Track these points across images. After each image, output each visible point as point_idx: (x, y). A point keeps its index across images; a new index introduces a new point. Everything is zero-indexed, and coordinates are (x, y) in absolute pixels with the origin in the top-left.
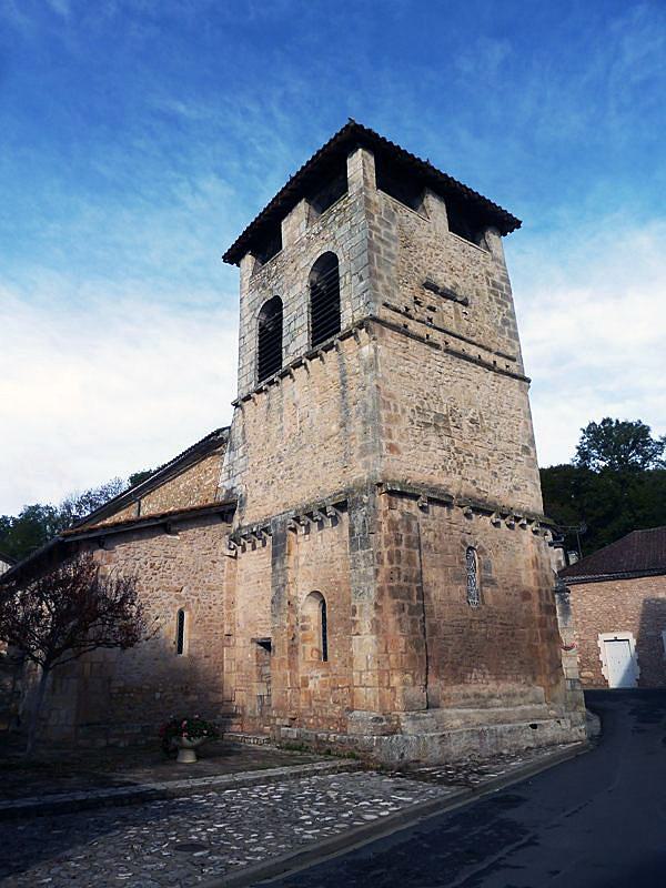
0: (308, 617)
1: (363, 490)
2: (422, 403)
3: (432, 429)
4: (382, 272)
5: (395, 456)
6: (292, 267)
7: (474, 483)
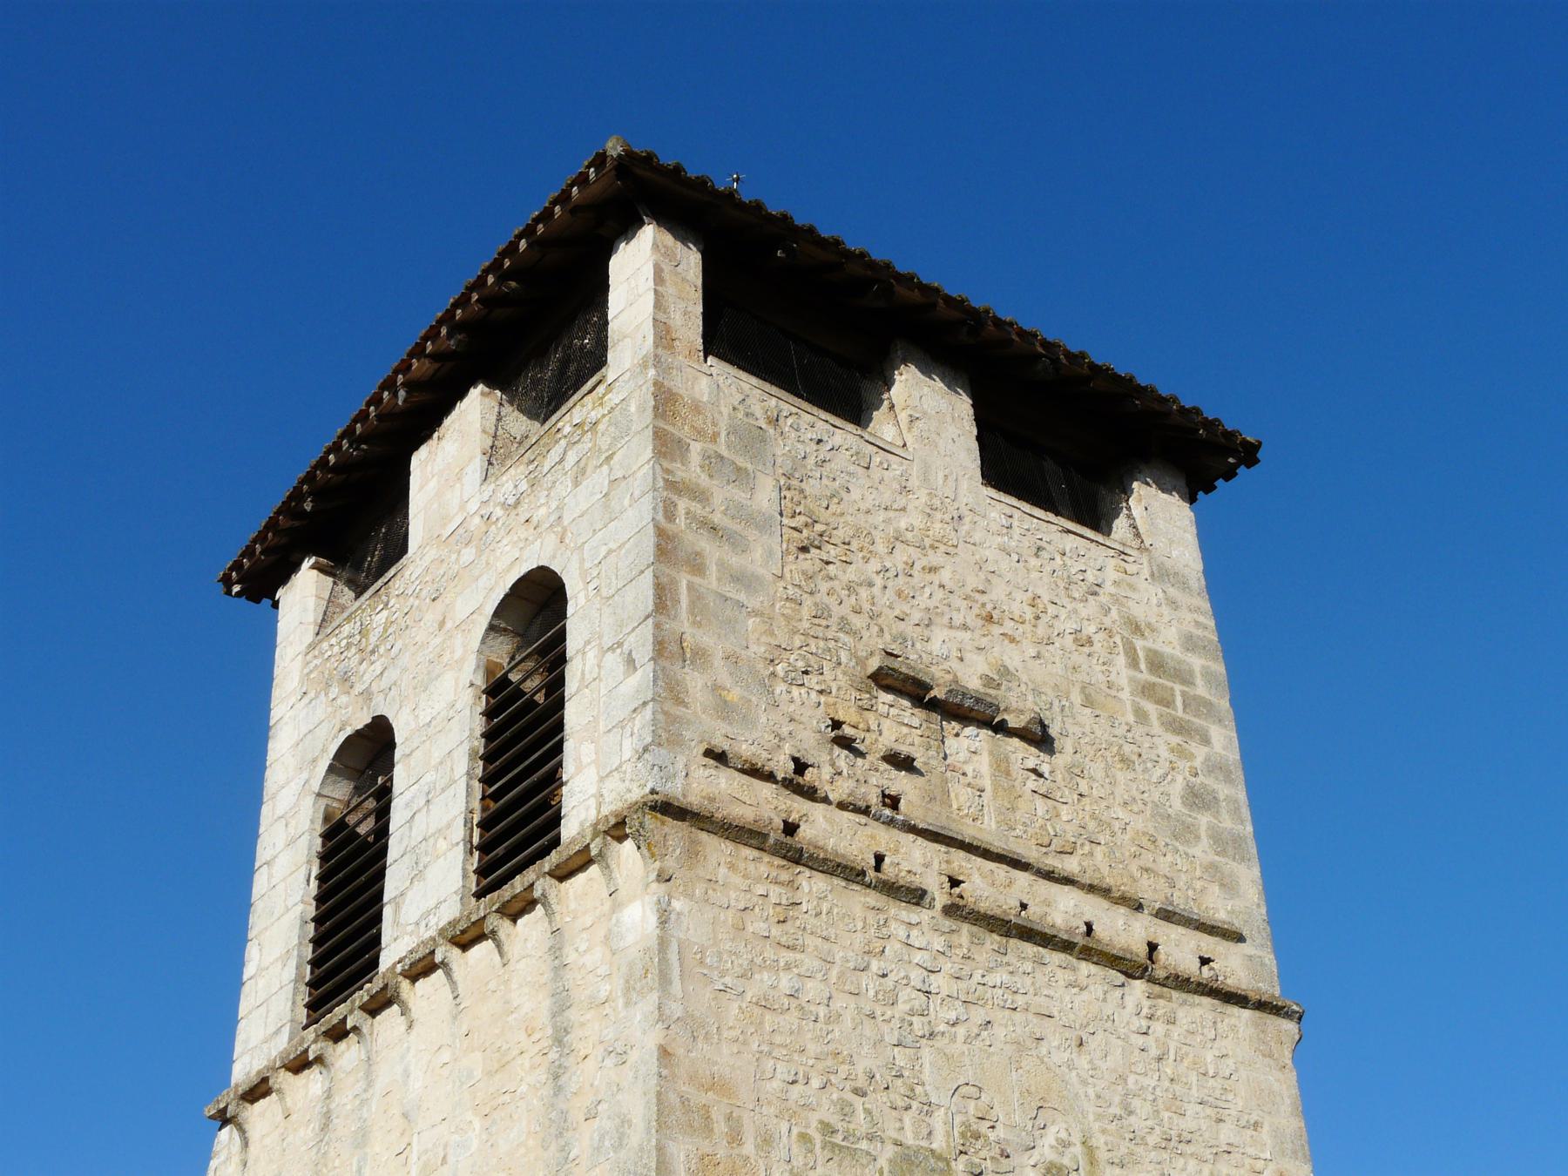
2: (846, 1111)
4: (707, 639)
6: (431, 617)
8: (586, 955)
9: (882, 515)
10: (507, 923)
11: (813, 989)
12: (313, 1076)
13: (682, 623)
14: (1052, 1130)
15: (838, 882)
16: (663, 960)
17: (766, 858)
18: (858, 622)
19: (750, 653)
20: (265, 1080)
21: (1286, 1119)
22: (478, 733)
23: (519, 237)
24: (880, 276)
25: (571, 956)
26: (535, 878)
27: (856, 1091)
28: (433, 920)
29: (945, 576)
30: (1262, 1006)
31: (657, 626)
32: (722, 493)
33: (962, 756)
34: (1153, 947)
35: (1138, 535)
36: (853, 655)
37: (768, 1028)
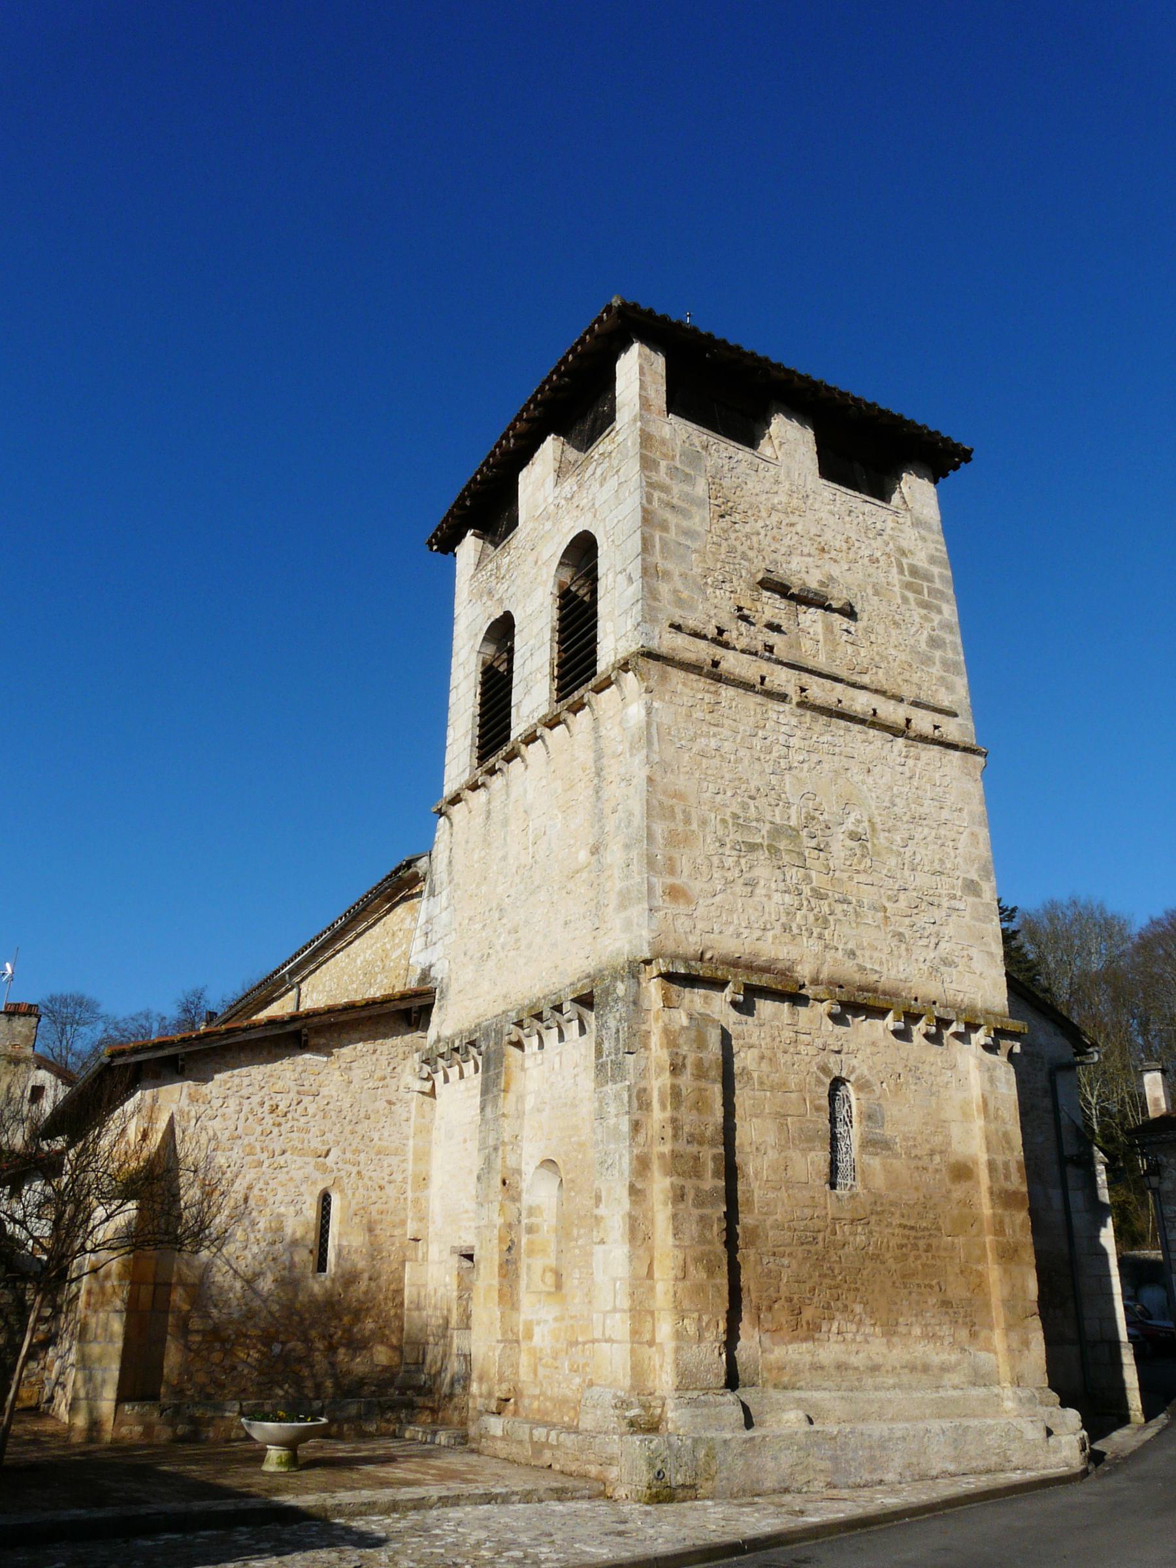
0: (539, 1207)
1: (616, 976)
2: (745, 807)
3: (762, 855)
4: (670, 566)
5: (682, 908)
6: (531, 559)
7: (852, 954)
8: (611, 731)
9: (764, 496)
10: (571, 715)
11: (727, 746)
12: (481, 792)
13: (657, 557)
14: (853, 815)
15: (741, 691)
16: (649, 733)
17: (703, 679)
18: (751, 554)
19: (693, 573)
20: (458, 795)
21: (977, 807)
22: (556, 618)
23: (568, 354)
24: (763, 365)
25: (603, 732)
26: (584, 692)
27: (751, 797)
28: (536, 715)
29: (799, 528)
30: (966, 749)
31: (643, 560)
32: (677, 488)
33: (807, 624)
34: (908, 721)
35: (905, 502)
36: (749, 572)
37: (704, 766)
